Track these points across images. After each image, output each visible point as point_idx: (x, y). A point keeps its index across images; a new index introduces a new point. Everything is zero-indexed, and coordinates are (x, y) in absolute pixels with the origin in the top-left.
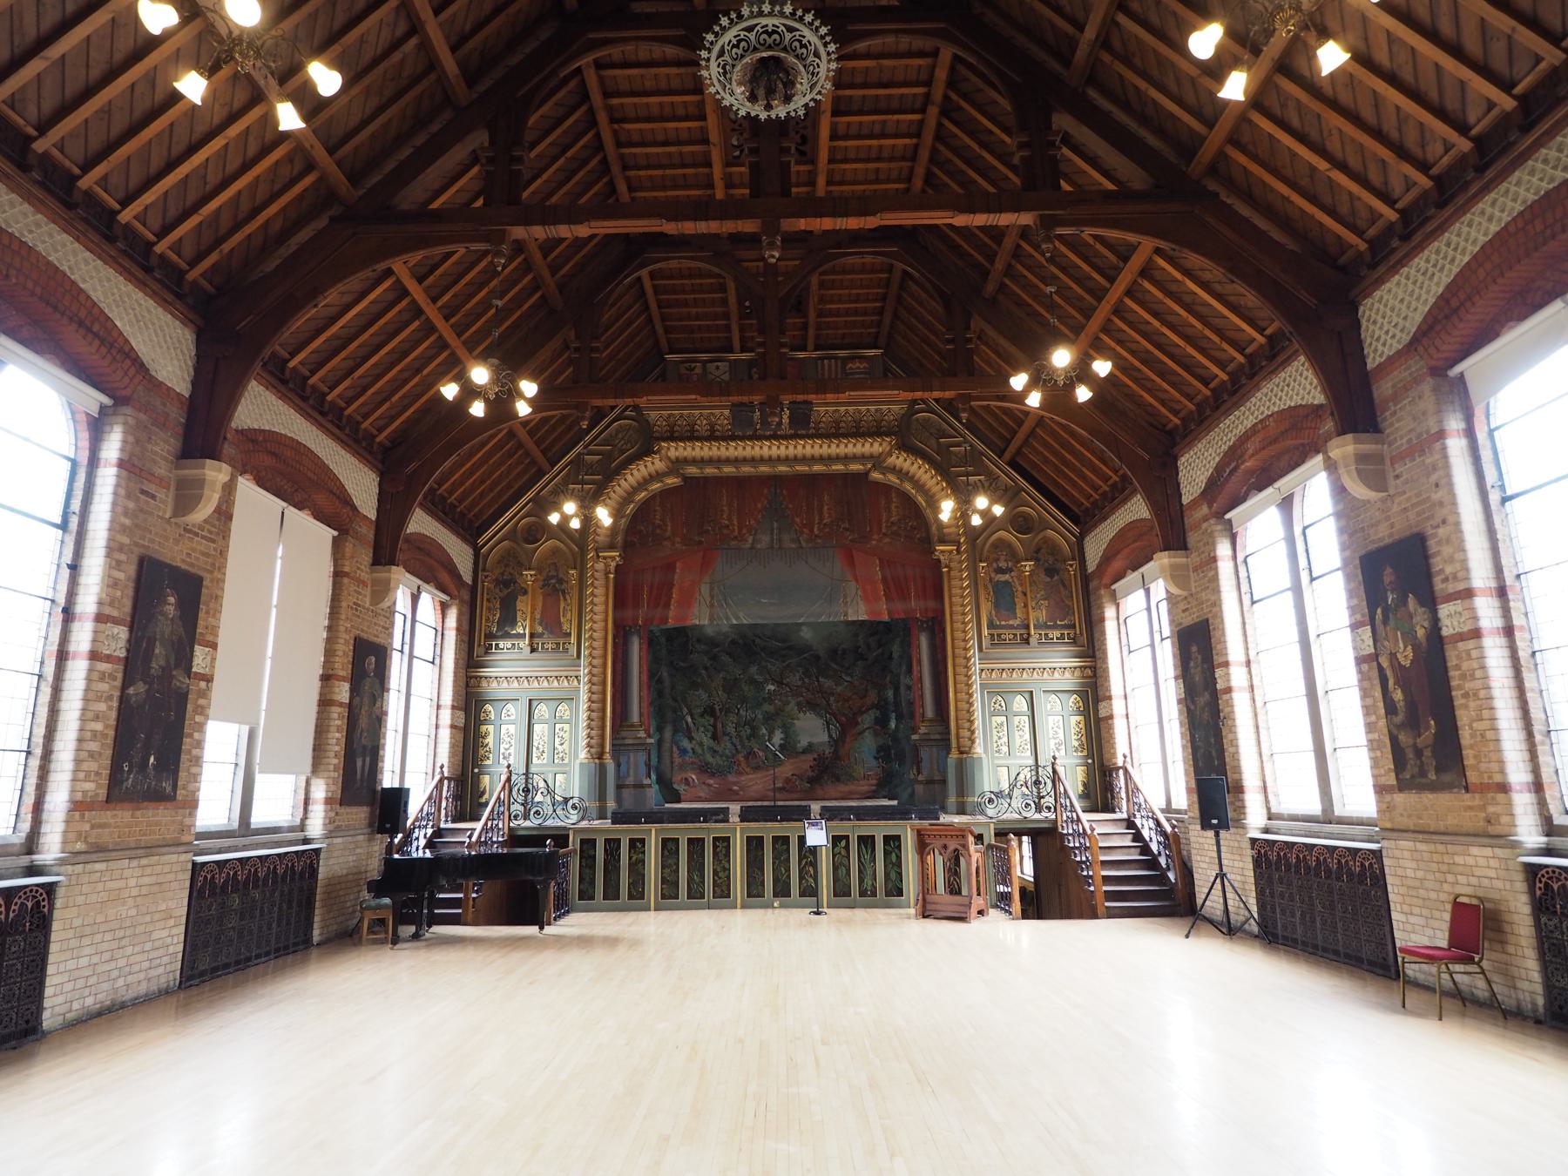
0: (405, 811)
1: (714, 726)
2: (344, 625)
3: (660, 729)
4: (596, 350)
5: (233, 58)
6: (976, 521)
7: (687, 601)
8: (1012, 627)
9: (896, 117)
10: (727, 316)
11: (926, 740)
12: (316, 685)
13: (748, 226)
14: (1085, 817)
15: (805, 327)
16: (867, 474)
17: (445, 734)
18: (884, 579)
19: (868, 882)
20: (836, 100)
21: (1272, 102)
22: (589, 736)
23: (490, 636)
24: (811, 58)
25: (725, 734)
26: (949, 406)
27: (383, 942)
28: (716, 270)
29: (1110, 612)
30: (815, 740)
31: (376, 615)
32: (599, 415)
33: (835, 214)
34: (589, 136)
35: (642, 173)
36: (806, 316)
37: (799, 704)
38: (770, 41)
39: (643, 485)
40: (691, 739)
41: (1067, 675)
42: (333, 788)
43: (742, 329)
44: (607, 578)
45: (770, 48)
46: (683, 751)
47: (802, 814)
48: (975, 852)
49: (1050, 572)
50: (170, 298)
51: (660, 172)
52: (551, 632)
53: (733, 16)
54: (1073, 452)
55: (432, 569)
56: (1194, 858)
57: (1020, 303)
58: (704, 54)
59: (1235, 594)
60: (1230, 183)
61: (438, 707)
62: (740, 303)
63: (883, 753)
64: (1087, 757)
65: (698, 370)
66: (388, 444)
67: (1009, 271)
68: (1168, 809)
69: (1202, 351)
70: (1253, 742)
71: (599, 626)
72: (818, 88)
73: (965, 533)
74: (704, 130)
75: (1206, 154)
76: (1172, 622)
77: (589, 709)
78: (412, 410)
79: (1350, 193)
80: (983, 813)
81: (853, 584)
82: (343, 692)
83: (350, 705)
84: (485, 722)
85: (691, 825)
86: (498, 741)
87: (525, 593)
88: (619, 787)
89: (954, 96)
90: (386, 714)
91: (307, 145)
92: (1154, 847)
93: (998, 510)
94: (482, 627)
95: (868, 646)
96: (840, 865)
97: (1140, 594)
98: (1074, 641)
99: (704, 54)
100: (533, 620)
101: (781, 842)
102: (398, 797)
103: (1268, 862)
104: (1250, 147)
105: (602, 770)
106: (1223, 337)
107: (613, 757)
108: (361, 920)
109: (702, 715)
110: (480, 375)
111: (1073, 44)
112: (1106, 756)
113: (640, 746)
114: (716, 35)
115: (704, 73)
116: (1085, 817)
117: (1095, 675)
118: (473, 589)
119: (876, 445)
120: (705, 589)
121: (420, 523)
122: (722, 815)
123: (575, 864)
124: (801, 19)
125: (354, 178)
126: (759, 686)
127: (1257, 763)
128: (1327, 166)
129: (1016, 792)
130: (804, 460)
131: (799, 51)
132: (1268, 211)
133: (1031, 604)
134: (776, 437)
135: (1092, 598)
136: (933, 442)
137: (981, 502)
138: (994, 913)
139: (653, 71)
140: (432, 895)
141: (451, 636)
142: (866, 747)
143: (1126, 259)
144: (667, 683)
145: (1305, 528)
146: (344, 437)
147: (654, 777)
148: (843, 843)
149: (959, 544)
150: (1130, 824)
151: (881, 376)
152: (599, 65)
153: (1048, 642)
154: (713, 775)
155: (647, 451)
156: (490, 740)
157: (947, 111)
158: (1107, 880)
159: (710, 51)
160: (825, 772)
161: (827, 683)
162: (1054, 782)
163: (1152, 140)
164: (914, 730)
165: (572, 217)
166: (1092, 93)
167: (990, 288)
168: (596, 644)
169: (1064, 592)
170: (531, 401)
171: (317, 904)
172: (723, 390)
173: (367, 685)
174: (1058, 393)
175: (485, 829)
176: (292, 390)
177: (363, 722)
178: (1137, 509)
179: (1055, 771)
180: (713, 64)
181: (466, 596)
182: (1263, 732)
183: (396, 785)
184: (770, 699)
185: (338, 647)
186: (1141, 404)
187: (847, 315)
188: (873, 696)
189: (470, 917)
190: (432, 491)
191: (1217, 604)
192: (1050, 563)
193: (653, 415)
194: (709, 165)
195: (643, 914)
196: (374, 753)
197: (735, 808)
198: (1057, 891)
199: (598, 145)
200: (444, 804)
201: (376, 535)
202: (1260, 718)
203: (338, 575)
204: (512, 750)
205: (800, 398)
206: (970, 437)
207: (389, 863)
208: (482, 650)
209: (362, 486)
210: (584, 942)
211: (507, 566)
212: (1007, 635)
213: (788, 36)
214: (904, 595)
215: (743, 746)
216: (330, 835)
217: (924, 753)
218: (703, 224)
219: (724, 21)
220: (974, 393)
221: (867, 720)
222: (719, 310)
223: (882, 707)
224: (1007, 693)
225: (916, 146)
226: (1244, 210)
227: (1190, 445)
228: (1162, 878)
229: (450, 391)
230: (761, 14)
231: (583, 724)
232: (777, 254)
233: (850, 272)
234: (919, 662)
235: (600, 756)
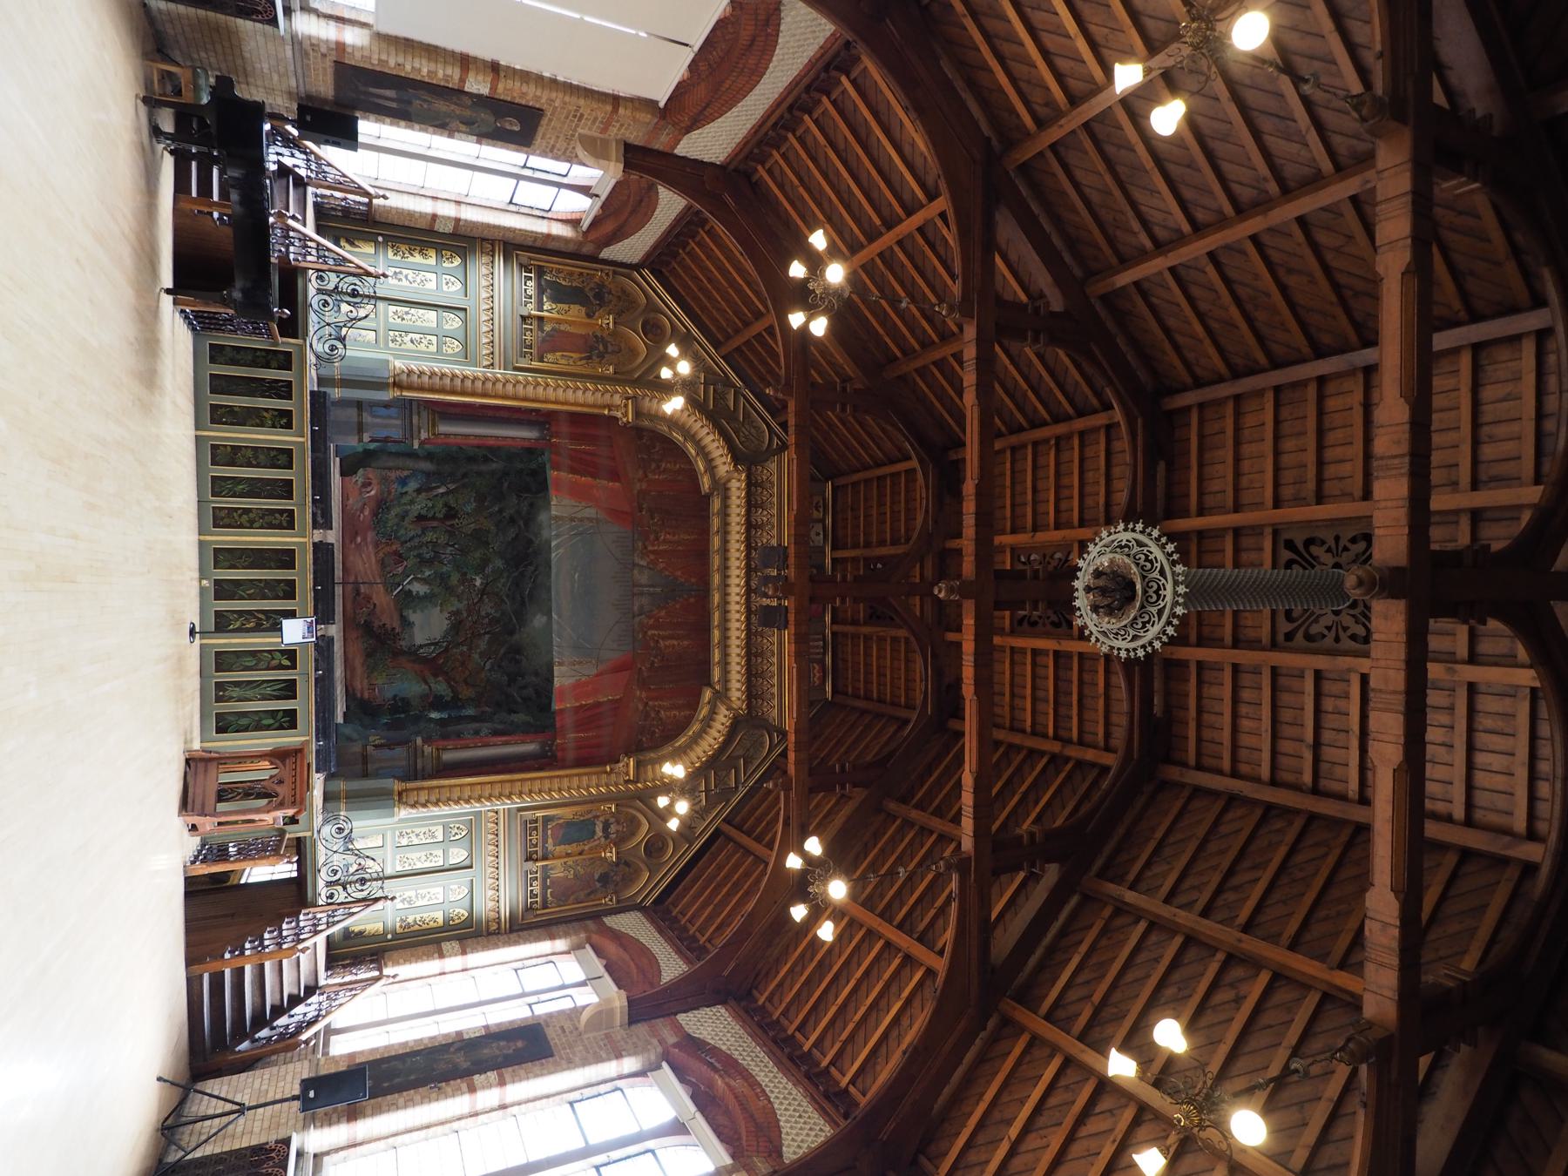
0: (327, 142)
1: (434, 518)
2: (558, 98)
3: (430, 456)
4: (843, 410)
5: (1193, 20)
6: (662, 802)
7: (577, 493)
8: (545, 841)
9: (1051, 712)
10: (868, 545)
11: (416, 753)
12: (487, 54)
13: (968, 567)
15: (855, 622)
16: (709, 684)
17: (426, 207)
18: (598, 705)
19: (236, 692)
20: (1094, 657)
21: (1105, 1103)
22: (422, 373)
23: (540, 272)
24: (1132, 632)
26: (777, 768)
27: (148, 84)
28: (915, 535)
29: (561, 944)
30: (416, 630)
31: (569, 139)
32: (776, 409)
33: (978, 654)
34: (1046, 416)
35: (1008, 465)
36: (865, 624)
37: (457, 613)
38: (1151, 592)
39: (702, 451)
40: (418, 491)
41: (491, 904)
42: (358, 55)
43: (855, 560)
44: (604, 407)
45: (1145, 592)
46: (403, 482)
47: (323, 613)
48: (273, 818)
49: (604, 879)
50: (827, 58)
51: (1008, 483)
52: (542, 341)
53: (1175, 557)
54: (729, 895)
55: (619, 212)
56: (267, 1071)
57: (876, 836)
58: (1139, 526)
59: (581, 1082)
60: (994, 1040)
61: (458, 203)
62: (880, 559)
63: (400, 706)
64: (394, 933)
65: (816, 515)
66: (755, 178)
67: (908, 824)
68: (329, 1031)
69: (832, 1022)
70: (410, 1125)
71: (551, 394)
72: (1102, 639)
73: (647, 787)
74: (1046, 528)
75: (1022, 1015)
76: (550, 1015)
77: (454, 376)
79: (987, 1162)
80: (326, 821)
81: (594, 672)
82: (478, 85)
83: (461, 92)
85: (309, 484)
86: (417, 269)
87: (589, 316)
88: (359, 405)
89: (1069, 766)
90: (451, 136)
91: (1062, 122)
92: (282, 1021)
93: (673, 825)
94: (552, 263)
95: (525, 687)
96: (255, 658)
97: (580, 976)
98: (528, 909)
99: (1139, 526)
100: (559, 321)
101: (289, 590)
102: (346, 136)
103: (260, 1164)
104: (1028, 1058)
105: (381, 385)
106: (845, 1043)
107: (396, 400)
108: (178, 65)
109: (446, 505)
110: (836, 274)
111: (1118, 879)
112: (395, 954)
113: (410, 432)
114: (1158, 540)
115: (1121, 526)
116: (320, 940)
117: (490, 934)
118: (593, 259)
119: (738, 694)
120: (590, 512)
121: (670, 204)
122: (322, 519)
123: (258, 343)
124: (1169, 623)
125: (1024, 168)
126: (480, 569)
127: (385, 1131)
128: (1013, 1138)
129: (351, 859)
130: (725, 620)
131: (1140, 621)
132: (968, 1081)
133: (570, 861)
134: (749, 591)
136: (741, 752)
137: (683, 807)
138: (194, 842)
139: (1103, 482)
140: (216, 161)
141: (541, 227)
142: (410, 687)
143: (920, 940)
144: (483, 468)
145: (652, 1151)
147: (373, 446)
148: (286, 663)
149: (635, 782)
150: (311, 990)
151: (808, 695)
152: (1110, 428)
153: (528, 882)
154: (375, 514)
155: (737, 458)
156: (417, 259)
157: (1056, 760)
158: (239, 974)
159: (1142, 532)
160: (377, 640)
161: (483, 644)
162: (364, 900)
163: (1033, 961)
164: (426, 741)
165: (983, 389)
166: (1074, 900)
167: (892, 806)
168: (530, 389)
169: (582, 895)
170: (805, 329)
171: (201, 12)
172: (801, 538)
173: (486, 116)
174: (801, 887)
175: (305, 239)
176: (817, 77)
177: (441, 106)
178: (672, 967)
179: (376, 900)
180: (1129, 535)
181: (587, 249)
182: (423, 1133)
183: (361, 139)
184: (464, 579)
185: (532, 87)
186: (779, 962)
187: (866, 665)
188: (466, 693)
190: (705, 221)
191: (571, 1064)
192: (613, 878)
193: (773, 466)
194: (1014, 531)
196: (401, 114)
197: (332, 537)
198: (221, 912)
199: (1036, 424)
200: (338, 194)
201: (658, 152)
202: (439, 1129)
203: (615, 100)
204: (405, 283)
205: (791, 617)
206: (742, 791)
207: (257, 111)
208: (525, 261)
209: (712, 142)
210: (149, 345)
212: (536, 838)
213: (1154, 610)
214: (581, 725)
215: (410, 549)
216: (296, 42)
217: (400, 751)
218: (972, 522)
219: (1170, 548)
220: (793, 794)
221: (441, 687)
222: (874, 539)
223: (455, 702)
224: (471, 840)
225: (1023, 731)
226: (969, 1057)
227: (737, 1016)
228: (240, 1033)
229: (818, 240)
230: (1176, 583)
231: (437, 367)
232: (941, 596)
233: (907, 669)
234: (506, 743)
235: (397, 385)
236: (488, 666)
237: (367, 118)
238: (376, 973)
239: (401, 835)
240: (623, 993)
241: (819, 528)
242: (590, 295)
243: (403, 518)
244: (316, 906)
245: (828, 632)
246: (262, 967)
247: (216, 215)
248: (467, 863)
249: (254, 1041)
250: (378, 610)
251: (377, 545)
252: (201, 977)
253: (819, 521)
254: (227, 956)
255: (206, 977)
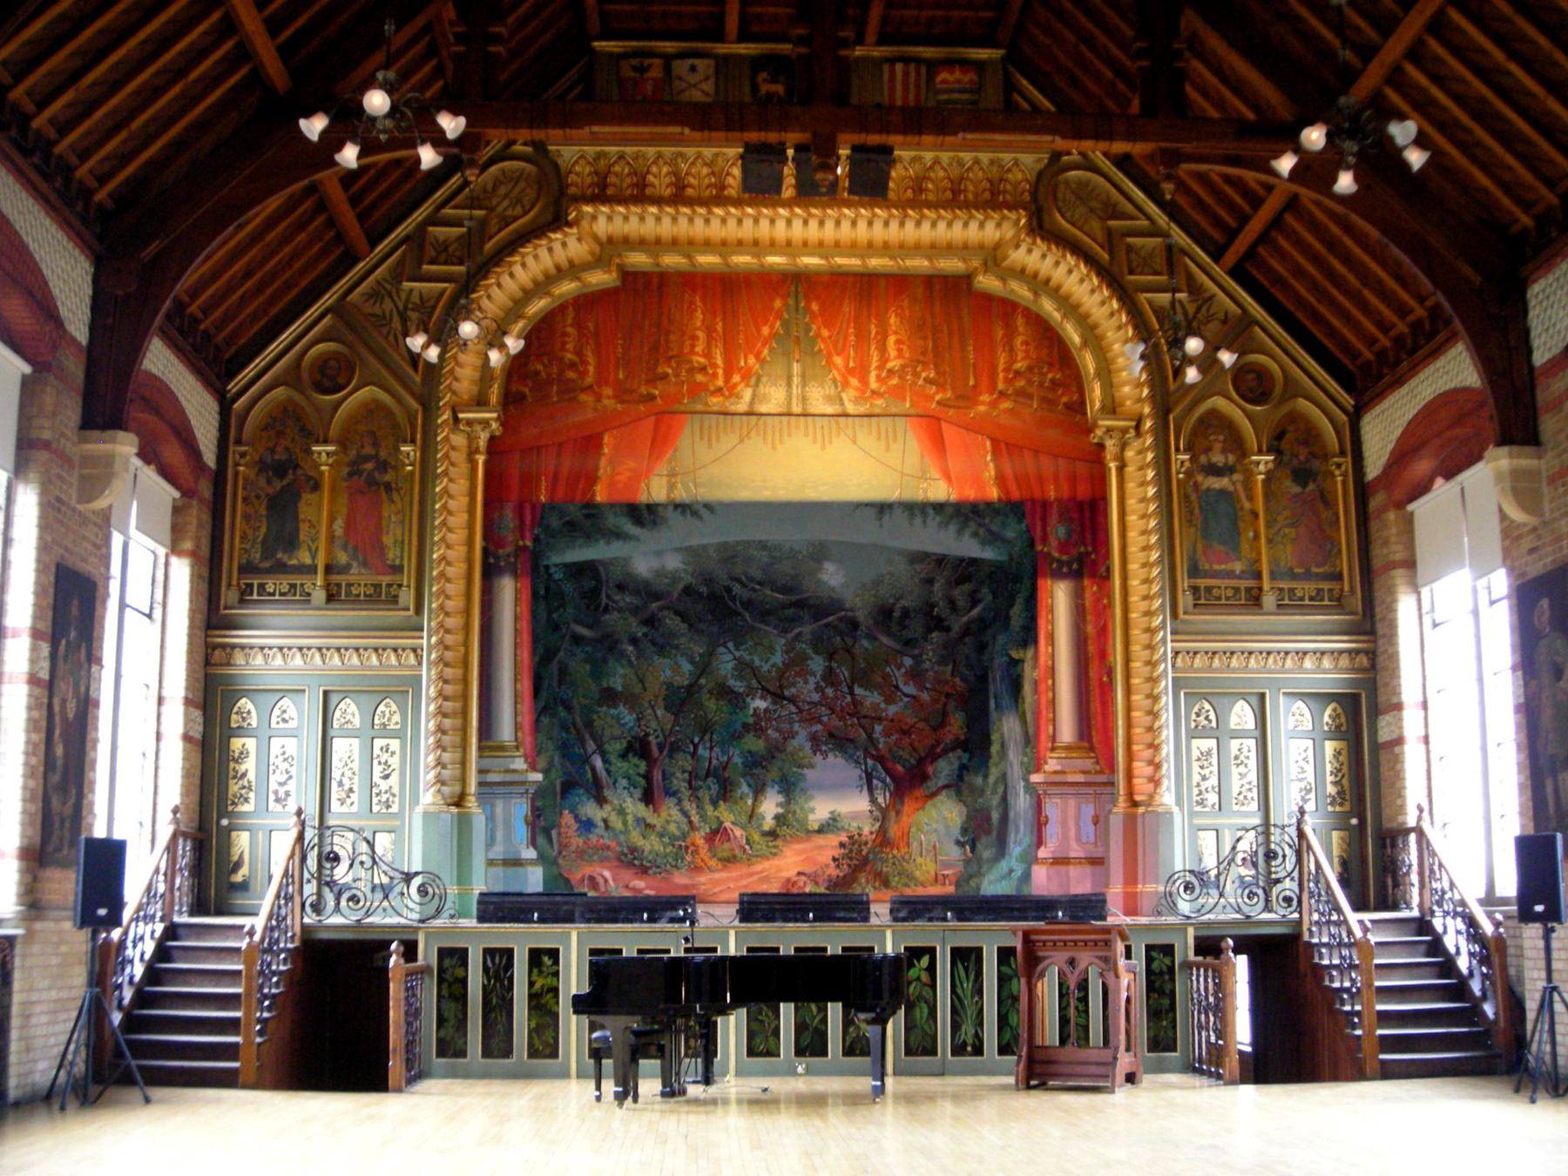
1: (648, 777)
8: (1230, 575)
14: (1353, 918)
16: (968, 278)
19: (968, 1031)
22: (440, 763)
25: (670, 793)
37: (814, 739)
39: (541, 286)
41: (1327, 663)
46: (587, 825)
49: (1302, 476)
54: (1347, 259)
65: (656, 72)
66: (110, 205)
68: (1490, 900)
71: (457, 554)
78: (159, 144)
84: (241, 732)
86: (265, 767)
92: (1463, 964)
109: (623, 756)
112: (1386, 812)
117: (1373, 666)
126: (735, 700)
135: (1374, 526)
136: (1095, 225)
146: (53, 197)
148: (925, 961)
150: (1422, 925)
154: (643, 871)
155: (557, 221)
156: (249, 766)
158: (1386, 1018)
161: (870, 698)
162: (1299, 854)
178: (1456, 369)
179: (1301, 835)
189: (252, 1078)
195: (558, 1084)
198: (1301, 1038)
204: (291, 786)
211: (280, 434)
215: (703, 817)
220: (1187, 148)
228: (1472, 1014)
231: (426, 741)
236: (910, 689)
237: (91, 826)
238: (1413, 837)
239: (1201, 803)
240: (1491, 452)
241: (681, 67)
242: (278, 485)
243: (648, 826)
244: (1299, 922)
245: (878, 52)
246: (1381, 990)
247: (258, 1040)
248: (1254, 701)
249: (1484, 997)
250: (808, 870)
251: (697, 869)
252: (1383, 1062)
253: (667, 69)
254: (1358, 1032)
255: (1382, 1056)
